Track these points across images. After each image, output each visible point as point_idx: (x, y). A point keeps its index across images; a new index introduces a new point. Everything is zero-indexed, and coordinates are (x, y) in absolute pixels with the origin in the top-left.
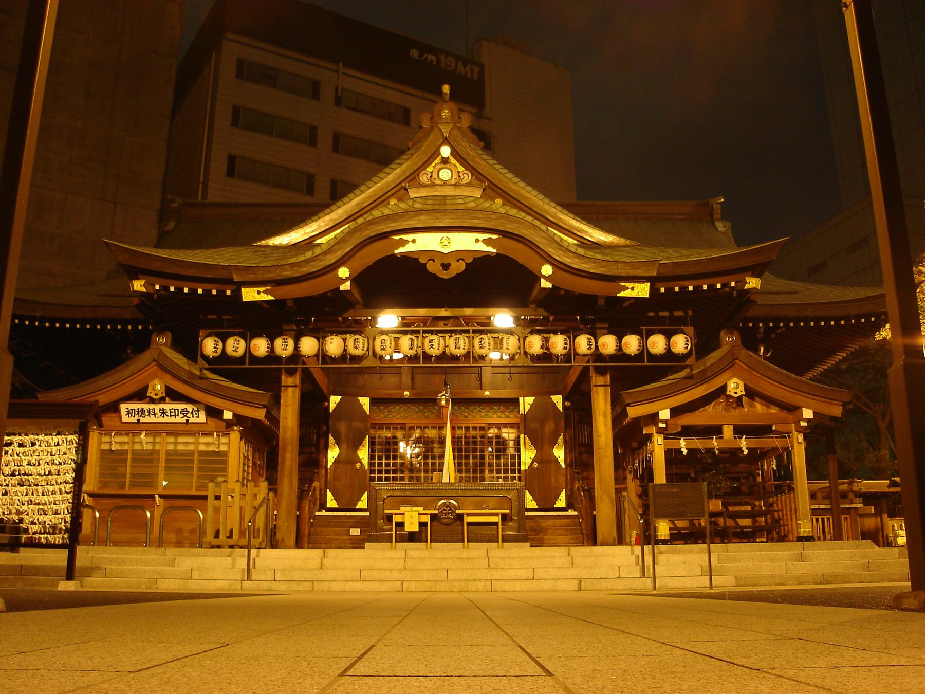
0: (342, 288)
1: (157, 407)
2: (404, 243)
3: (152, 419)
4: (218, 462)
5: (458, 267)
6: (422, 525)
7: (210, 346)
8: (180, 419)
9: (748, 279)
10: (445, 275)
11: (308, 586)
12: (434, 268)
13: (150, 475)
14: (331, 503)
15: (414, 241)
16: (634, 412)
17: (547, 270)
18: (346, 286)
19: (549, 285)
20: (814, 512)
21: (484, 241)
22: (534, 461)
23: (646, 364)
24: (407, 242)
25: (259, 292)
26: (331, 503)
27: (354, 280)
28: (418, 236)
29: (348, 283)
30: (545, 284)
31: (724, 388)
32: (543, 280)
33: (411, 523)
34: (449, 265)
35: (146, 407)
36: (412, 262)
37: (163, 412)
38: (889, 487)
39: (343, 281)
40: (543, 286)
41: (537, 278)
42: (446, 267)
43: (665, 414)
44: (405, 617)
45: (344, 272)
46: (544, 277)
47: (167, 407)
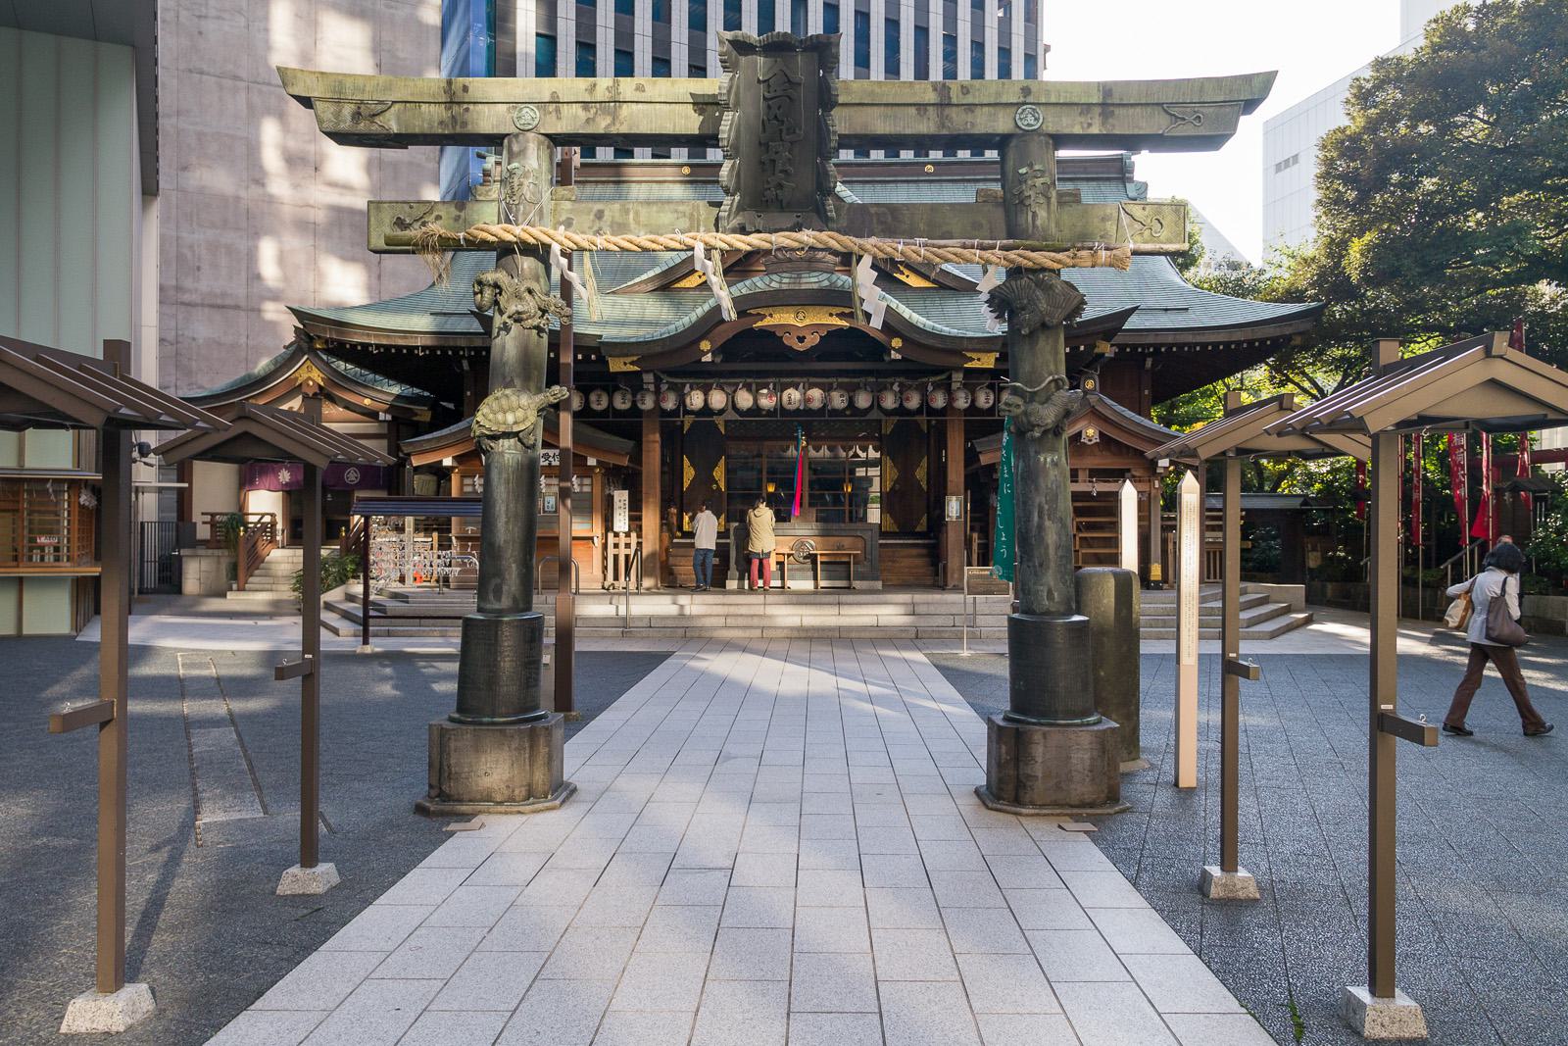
0: (703, 360)
4: (1090, 527)
10: (800, 347)
11: (757, 633)
12: (791, 341)
13: (1175, 519)
16: (984, 460)
17: (897, 343)
18: (708, 358)
19: (899, 357)
20: (851, 520)
21: (838, 315)
22: (896, 482)
24: (764, 316)
25: (625, 364)
30: (895, 355)
31: (1079, 434)
34: (804, 338)
36: (769, 334)
38: (1301, 505)
39: (705, 353)
42: (801, 339)
44: (474, 951)
45: (705, 345)
46: (894, 349)
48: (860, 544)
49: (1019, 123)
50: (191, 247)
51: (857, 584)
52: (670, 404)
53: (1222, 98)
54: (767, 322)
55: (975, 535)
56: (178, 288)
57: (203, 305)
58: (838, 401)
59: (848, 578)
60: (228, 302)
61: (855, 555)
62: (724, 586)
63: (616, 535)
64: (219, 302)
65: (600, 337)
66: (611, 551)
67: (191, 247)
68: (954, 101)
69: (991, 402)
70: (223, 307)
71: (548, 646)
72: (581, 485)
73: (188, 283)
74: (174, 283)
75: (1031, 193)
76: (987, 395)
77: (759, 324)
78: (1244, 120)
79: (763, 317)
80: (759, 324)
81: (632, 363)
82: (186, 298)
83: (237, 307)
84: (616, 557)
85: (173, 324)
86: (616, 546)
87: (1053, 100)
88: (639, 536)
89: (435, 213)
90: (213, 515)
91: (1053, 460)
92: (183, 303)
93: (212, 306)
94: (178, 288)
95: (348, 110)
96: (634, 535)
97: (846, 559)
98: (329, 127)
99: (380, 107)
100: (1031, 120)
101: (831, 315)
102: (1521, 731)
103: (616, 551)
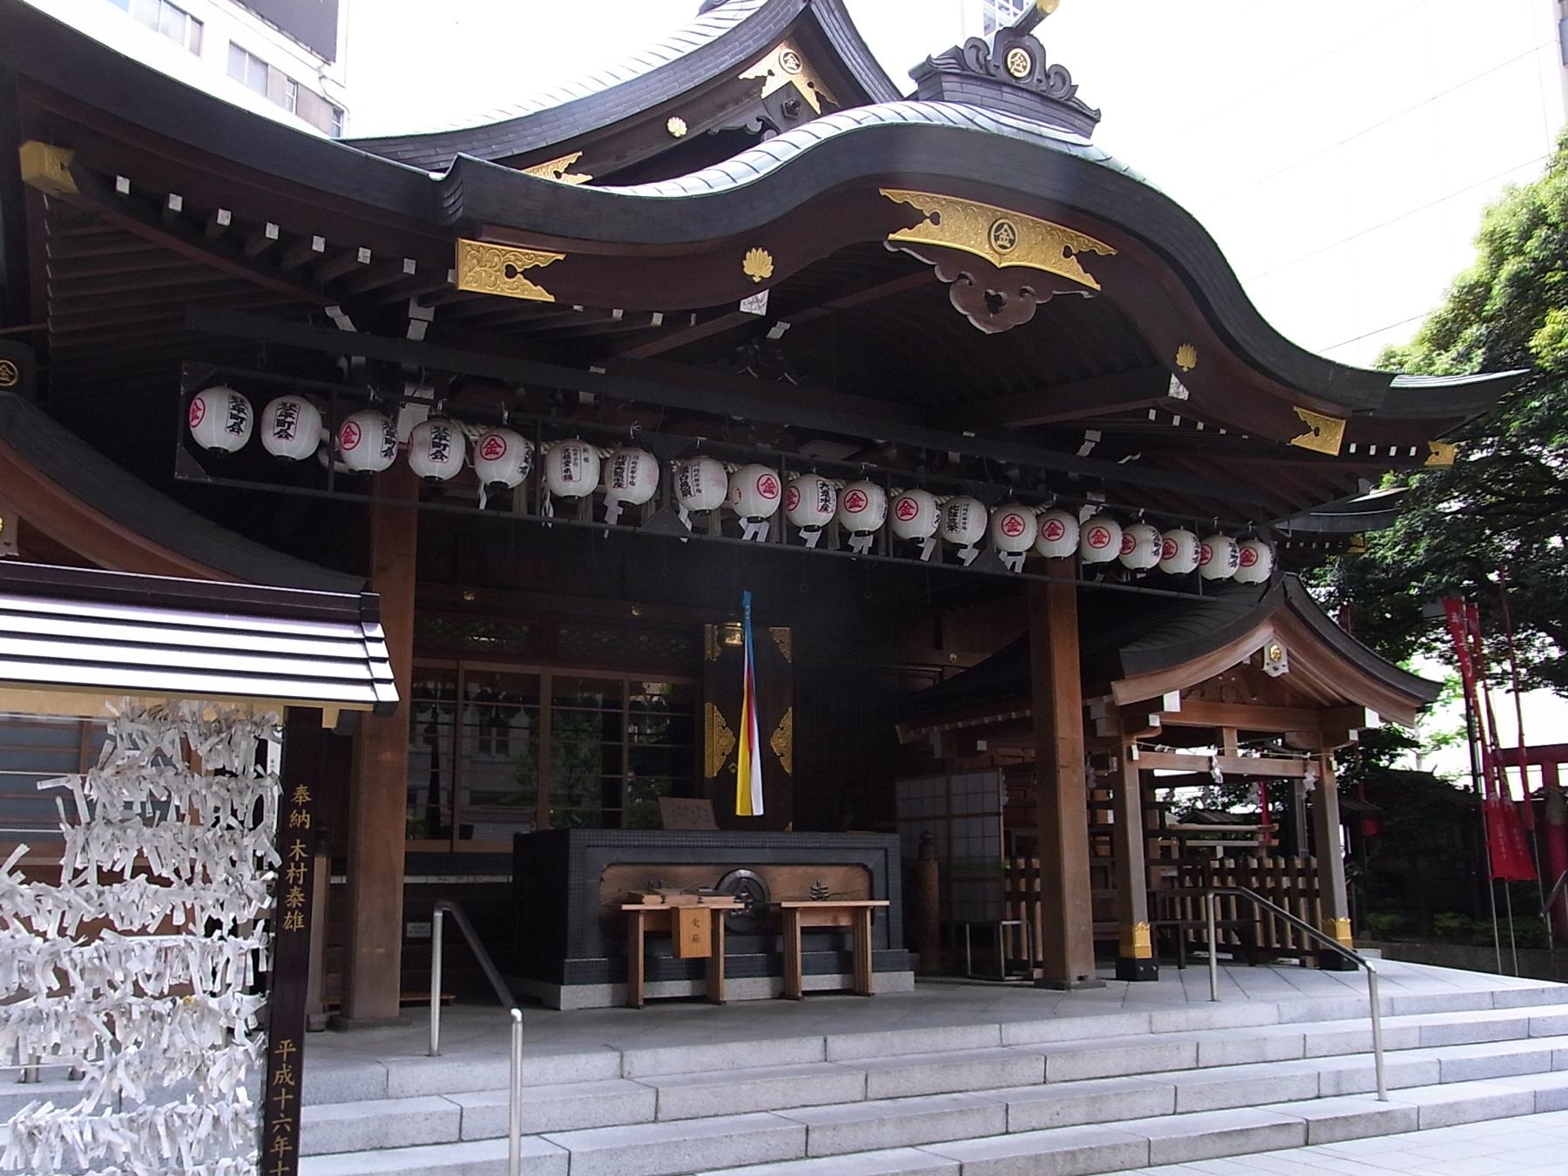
2: (911, 218)
5: (1022, 309)
7: (215, 425)
9: (1433, 446)
15: (935, 219)
17: (1186, 359)
23: (1201, 597)
27: (783, 295)
29: (763, 296)
32: (1174, 379)
33: (695, 939)
39: (752, 288)
40: (1172, 391)
41: (1163, 371)
43: (1172, 702)
48: (861, 883)
51: (879, 982)
61: (873, 909)
77: (903, 235)
80: (903, 235)
81: (533, 275)
88: (339, 864)
101: (1067, 253)
103: (695, 930)
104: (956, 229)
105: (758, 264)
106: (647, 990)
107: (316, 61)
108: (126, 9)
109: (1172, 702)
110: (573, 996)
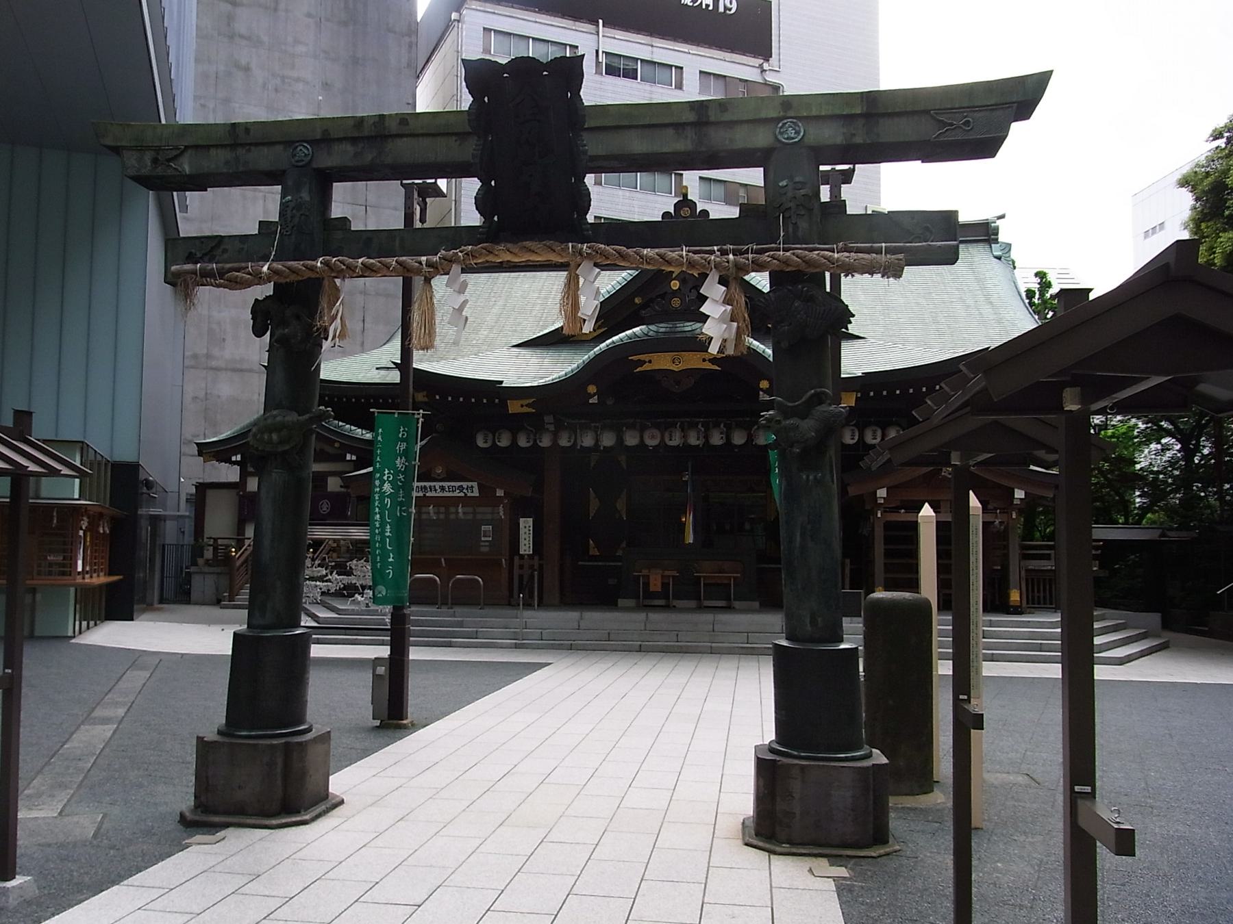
1: (437, 485)
3: (433, 494)
6: (665, 585)
8: (457, 494)
14: (594, 551)
18: (594, 400)
26: (594, 551)
28: (654, 356)
35: (427, 484)
37: (443, 488)
39: (592, 396)
47: (446, 484)
49: (780, 137)
50: (219, 323)
51: (737, 604)
52: (564, 442)
53: (993, 102)
54: (646, 367)
55: (848, 561)
56: (209, 356)
57: (226, 369)
58: (717, 439)
59: (728, 599)
60: (245, 366)
62: (616, 605)
63: (522, 557)
64: (238, 366)
65: (501, 382)
66: (516, 572)
67: (219, 323)
68: (712, 119)
69: (857, 438)
70: (242, 370)
71: (943, 657)
72: (437, 513)
73: (216, 352)
74: (205, 351)
75: (791, 205)
76: (874, 432)
78: (1016, 127)
79: (642, 363)
82: (214, 363)
83: (251, 371)
84: (521, 577)
85: (203, 385)
86: (521, 567)
87: (814, 113)
89: (222, 247)
90: (215, 540)
91: (815, 478)
92: (212, 369)
93: (234, 370)
94: (209, 356)
95: (148, 157)
96: (536, 558)
97: (726, 582)
98: (132, 172)
99: (175, 153)
100: (791, 133)
102: (741, 799)
104: (662, 362)
105: (592, 389)
106: (707, 603)
107: (757, 62)
108: (636, 78)
109: (882, 493)
110: (621, 602)
